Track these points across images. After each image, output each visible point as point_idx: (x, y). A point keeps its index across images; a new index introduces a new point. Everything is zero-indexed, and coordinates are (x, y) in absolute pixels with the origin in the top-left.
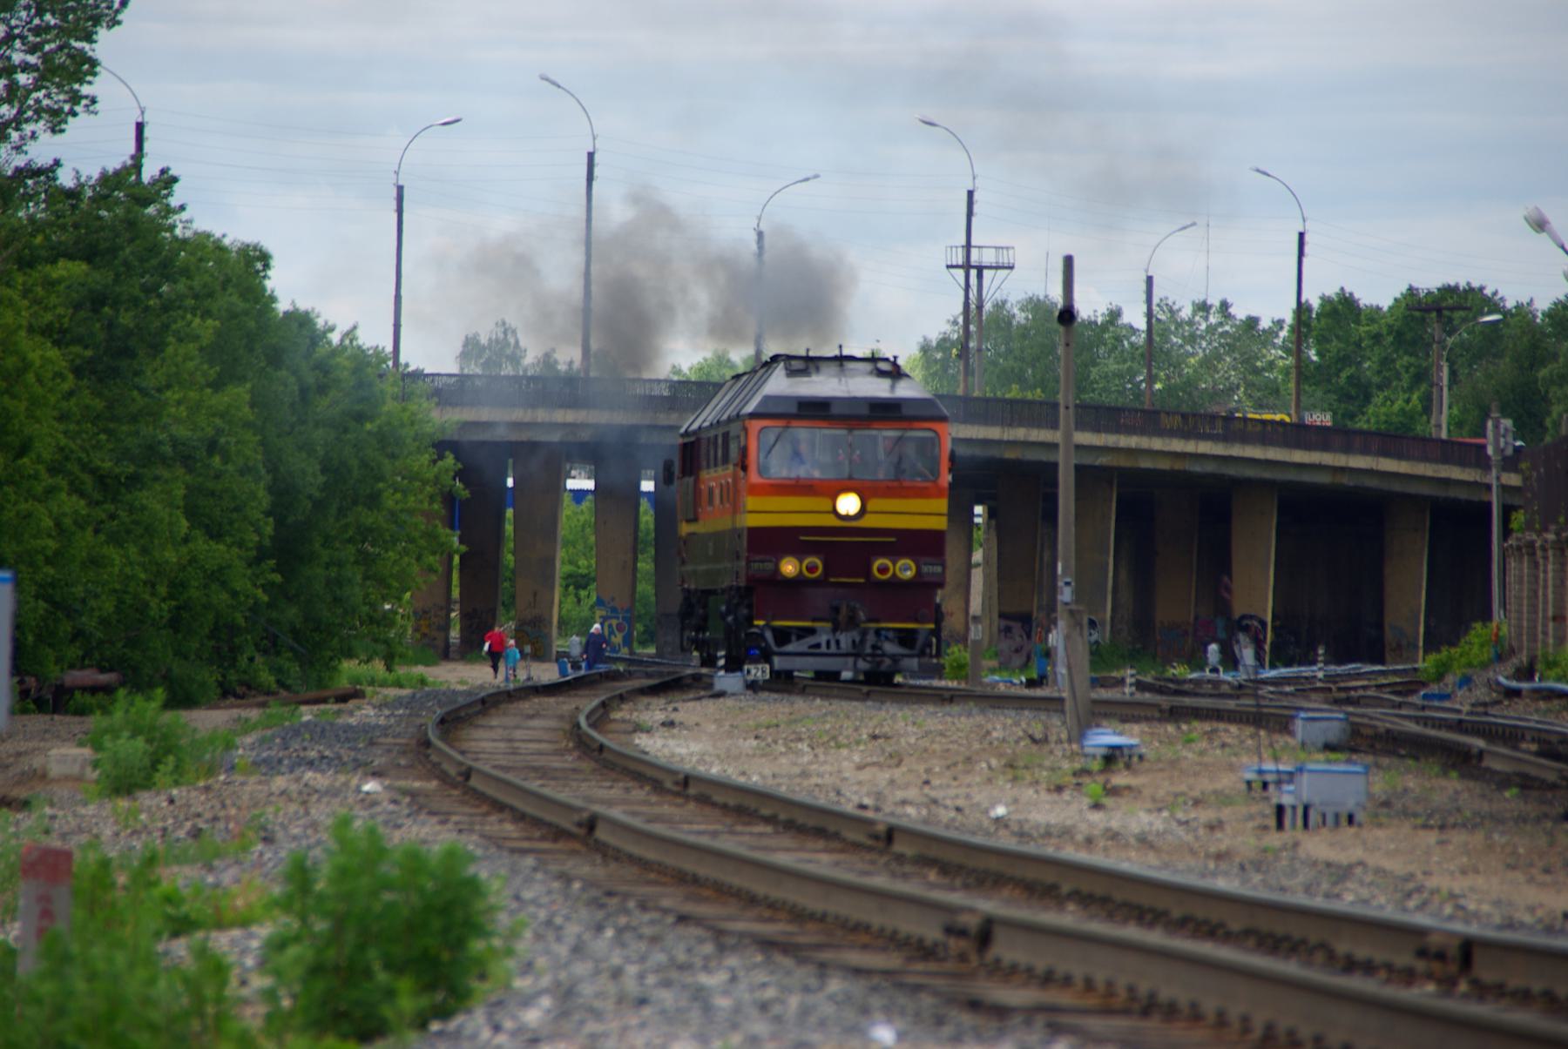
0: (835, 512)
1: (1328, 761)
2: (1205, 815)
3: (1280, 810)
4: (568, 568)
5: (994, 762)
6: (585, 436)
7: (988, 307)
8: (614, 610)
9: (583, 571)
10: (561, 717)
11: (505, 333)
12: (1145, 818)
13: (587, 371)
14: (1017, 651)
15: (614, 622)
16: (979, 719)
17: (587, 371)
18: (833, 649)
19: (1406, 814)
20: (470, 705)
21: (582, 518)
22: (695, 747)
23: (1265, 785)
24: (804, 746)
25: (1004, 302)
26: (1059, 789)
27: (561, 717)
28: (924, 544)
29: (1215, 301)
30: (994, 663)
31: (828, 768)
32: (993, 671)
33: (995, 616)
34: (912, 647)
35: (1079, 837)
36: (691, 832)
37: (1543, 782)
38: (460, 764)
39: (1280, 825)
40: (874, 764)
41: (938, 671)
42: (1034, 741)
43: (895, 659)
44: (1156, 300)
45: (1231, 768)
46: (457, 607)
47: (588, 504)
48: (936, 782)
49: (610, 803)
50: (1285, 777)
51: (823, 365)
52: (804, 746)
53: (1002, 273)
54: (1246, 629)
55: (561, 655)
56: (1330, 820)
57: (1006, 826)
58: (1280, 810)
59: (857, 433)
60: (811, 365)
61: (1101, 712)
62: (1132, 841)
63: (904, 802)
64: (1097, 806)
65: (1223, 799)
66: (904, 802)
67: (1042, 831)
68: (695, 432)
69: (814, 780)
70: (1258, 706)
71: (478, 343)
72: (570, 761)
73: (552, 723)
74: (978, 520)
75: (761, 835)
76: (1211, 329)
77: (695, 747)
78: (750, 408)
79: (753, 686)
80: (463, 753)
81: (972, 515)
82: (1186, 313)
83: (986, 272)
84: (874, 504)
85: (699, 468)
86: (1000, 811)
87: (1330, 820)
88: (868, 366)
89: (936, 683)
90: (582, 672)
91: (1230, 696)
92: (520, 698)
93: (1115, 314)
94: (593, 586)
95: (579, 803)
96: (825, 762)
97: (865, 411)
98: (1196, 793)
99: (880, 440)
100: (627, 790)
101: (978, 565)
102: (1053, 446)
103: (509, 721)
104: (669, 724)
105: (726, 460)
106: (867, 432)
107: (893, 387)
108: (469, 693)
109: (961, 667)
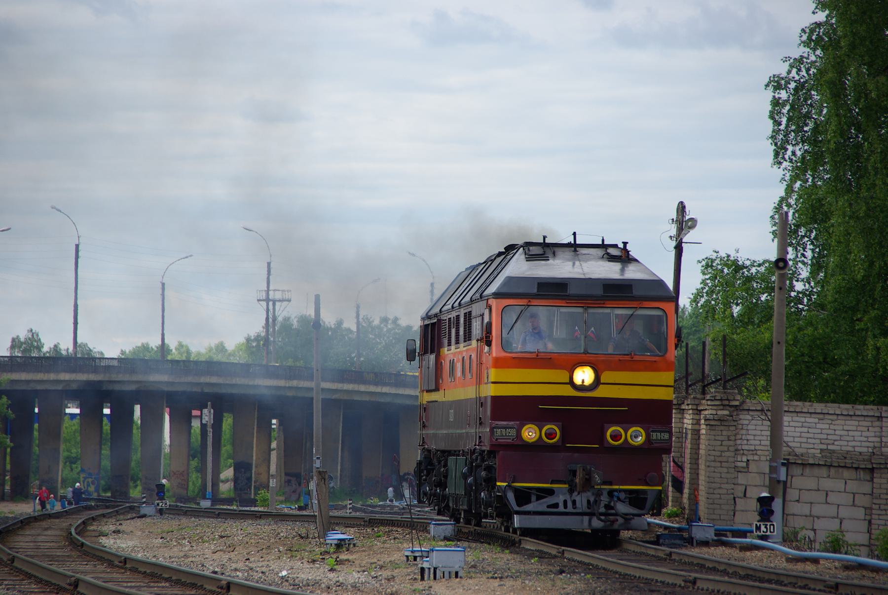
0: (571, 382)
1: (446, 546)
2: (386, 573)
3: (423, 569)
4: (66, 454)
5: (281, 548)
6: (74, 386)
7: (280, 319)
8: (90, 474)
9: (74, 455)
10: (61, 529)
11: (33, 335)
12: (356, 575)
13: (75, 354)
14: (294, 492)
15: (90, 480)
16: (274, 527)
17: (75, 354)
18: (570, 509)
19: (484, 571)
20: (14, 524)
21: (74, 428)
22: (130, 543)
23: (415, 558)
24: (185, 542)
25: (289, 318)
26: (314, 561)
27: (61, 529)
28: (655, 414)
29: (391, 317)
30: (282, 498)
31: (198, 553)
32: (281, 502)
33: (283, 474)
34: (641, 507)
35: (323, 586)
36: (127, 587)
37: (550, 554)
38: (9, 554)
39: (422, 579)
40: (221, 550)
41: (253, 503)
42: (302, 538)
43: (627, 518)
44: (361, 317)
45: (399, 550)
46: (8, 474)
47: (76, 421)
48: (252, 559)
49: (85, 573)
50: (425, 554)
51: (559, 251)
52: (185, 542)
53: (285, 303)
54: (406, 480)
55: (63, 497)
56: (447, 575)
57: (287, 581)
58: (423, 569)
59: (591, 311)
60: (549, 253)
61: (331, 524)
62: (349, 587)
63: (236, 570)
64: (332, 570)
65: (394, 565)
66: (236, 570)
67: (305, 583)
68: (436, 315)
69: (190, 559)
70: (411, 518)
71: (19, 341)
72: (66, 552)
73: (58, 533)
74: (273, 427)
75: (163, 587)
76: (389, 331)
77: (130, 543)
78: (493, 288)
79: (161, 512)
80: (10, 549)
81: (271, 424)
82: (376, 322)
83: (278, 304)
84: (606, 377)
85: (440, 346)
86: (284, 573)
87: (447, 575)
88: (599, 252)
89: (253, 509)
90: (74, 506)
91: (398, 514)
92: (41, 520)
93: (340, 323)
94: (79, 462)
95: (70, 573)
96: (197, 550)
97: (599, 292)
98: (381, 563)
99: (613, 317)
100: (95, 566)
101: (274, 449)
102: (311, 389)
103: (33, 532)
104: (117, 532)
105: (468, 337)
106: (601, 311)
107: (622, 271)
108: (14, 518)
109: (265, 500)
